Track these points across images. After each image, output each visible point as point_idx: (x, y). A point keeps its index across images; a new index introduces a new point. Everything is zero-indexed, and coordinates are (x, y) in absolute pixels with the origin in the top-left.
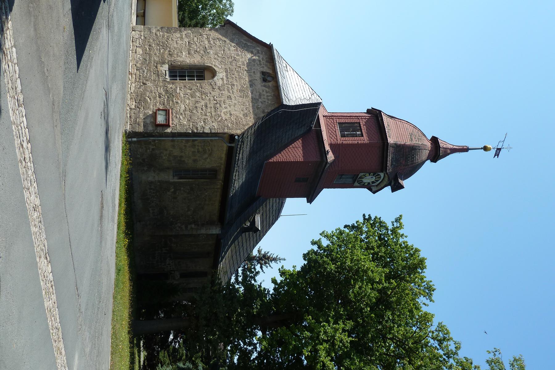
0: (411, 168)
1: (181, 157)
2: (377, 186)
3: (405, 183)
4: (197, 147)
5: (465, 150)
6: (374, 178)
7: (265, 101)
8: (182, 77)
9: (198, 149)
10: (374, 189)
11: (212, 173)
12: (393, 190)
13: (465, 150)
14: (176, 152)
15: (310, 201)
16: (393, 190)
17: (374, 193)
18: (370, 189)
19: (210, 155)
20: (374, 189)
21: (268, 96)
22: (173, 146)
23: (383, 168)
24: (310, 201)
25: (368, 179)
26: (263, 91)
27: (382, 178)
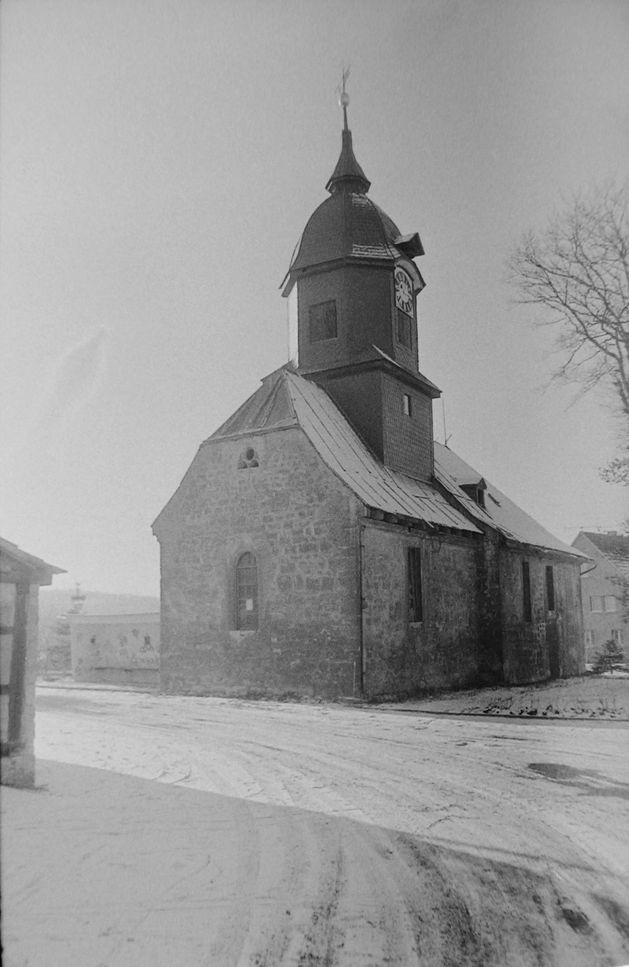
0: (374, 225)
1: (391, 608)
2: (413, 280)
3: (261, 384)
4: (377, 581)
5: (347, 136)
6: (402, 283)
7: (295, 463)
8: (553, 604)
9: (379, 578)
10: (418, 285)
11: (413, 555)
12: (421, 253)
13: (347, 136)
14: (385, 615)
15: (436, 393)
16: (421, 253)
17: (424, 285)
18: (419, 290)
19: (386, 557)
20: (418, 285)
21: (284, 458)
22: (376, 621)
23: (388, 265)
24: (436, 393)
25: (403, 294)
26: (275, 466)
27: (401, 270)
